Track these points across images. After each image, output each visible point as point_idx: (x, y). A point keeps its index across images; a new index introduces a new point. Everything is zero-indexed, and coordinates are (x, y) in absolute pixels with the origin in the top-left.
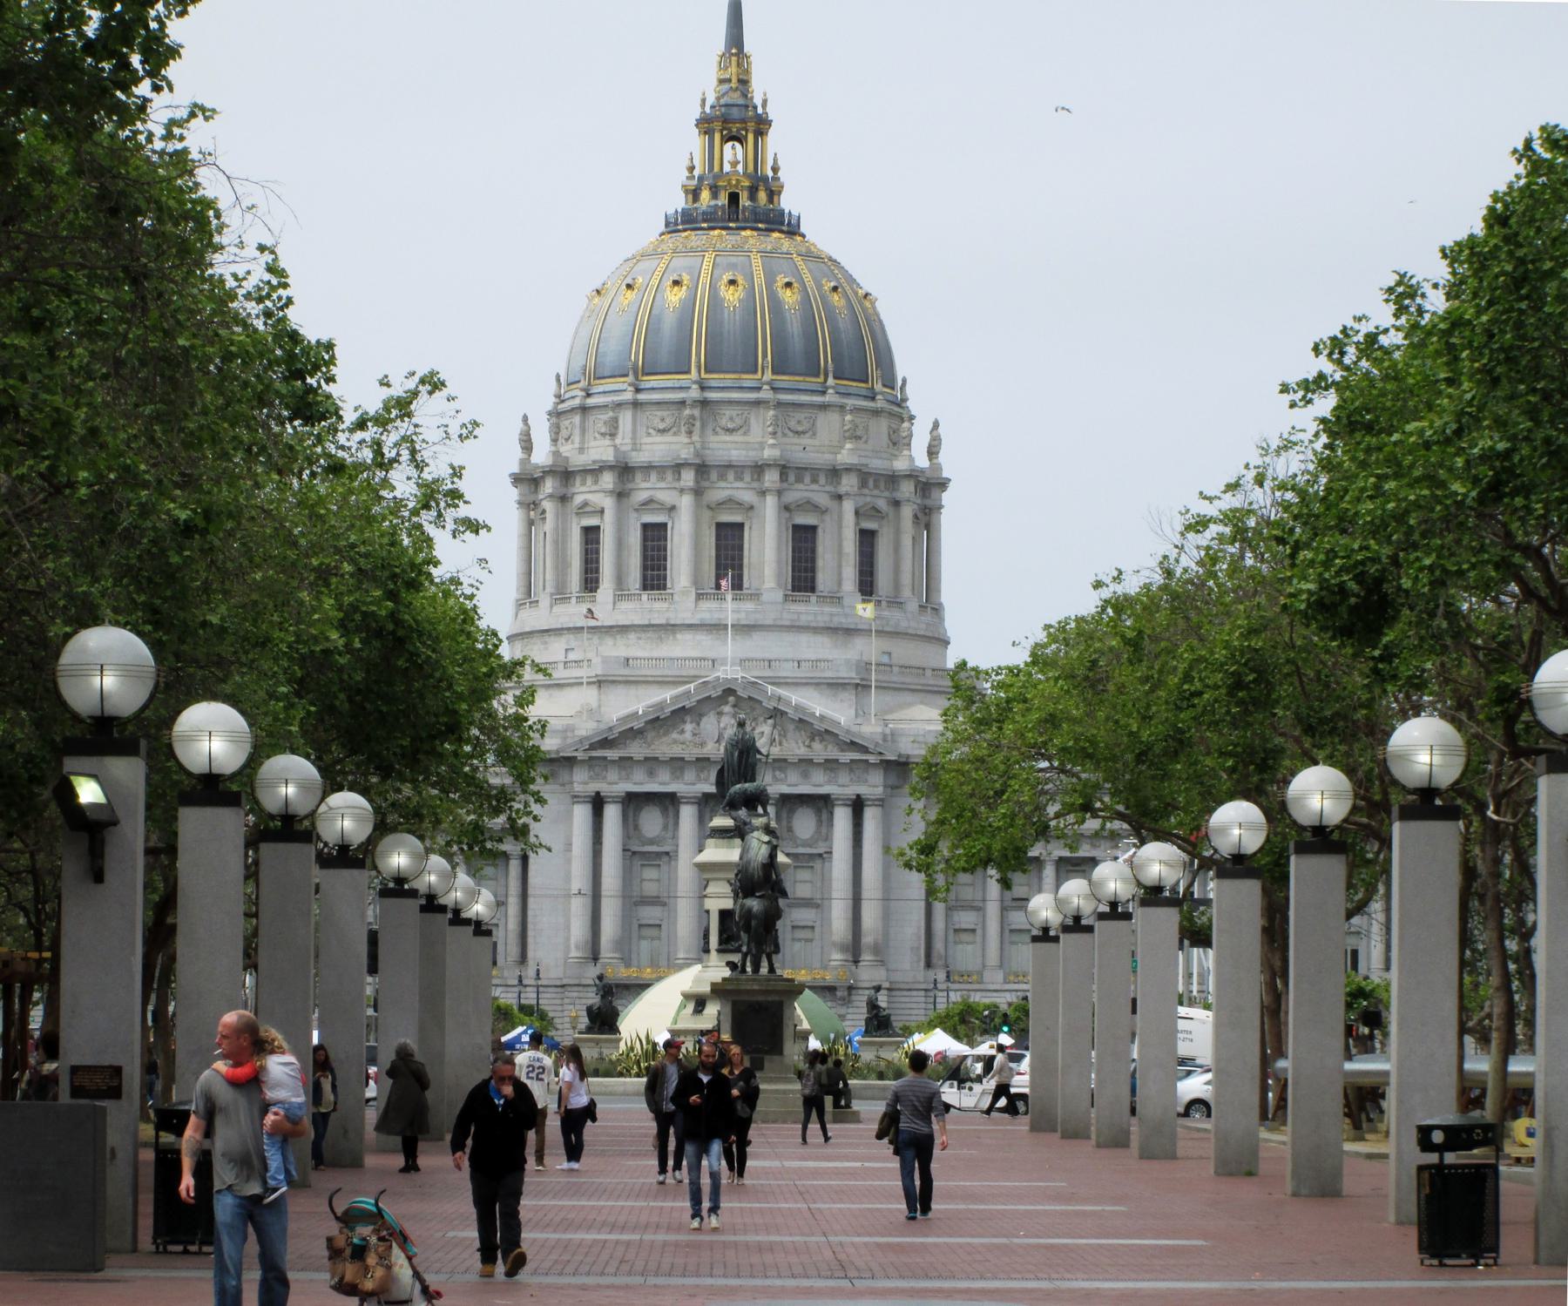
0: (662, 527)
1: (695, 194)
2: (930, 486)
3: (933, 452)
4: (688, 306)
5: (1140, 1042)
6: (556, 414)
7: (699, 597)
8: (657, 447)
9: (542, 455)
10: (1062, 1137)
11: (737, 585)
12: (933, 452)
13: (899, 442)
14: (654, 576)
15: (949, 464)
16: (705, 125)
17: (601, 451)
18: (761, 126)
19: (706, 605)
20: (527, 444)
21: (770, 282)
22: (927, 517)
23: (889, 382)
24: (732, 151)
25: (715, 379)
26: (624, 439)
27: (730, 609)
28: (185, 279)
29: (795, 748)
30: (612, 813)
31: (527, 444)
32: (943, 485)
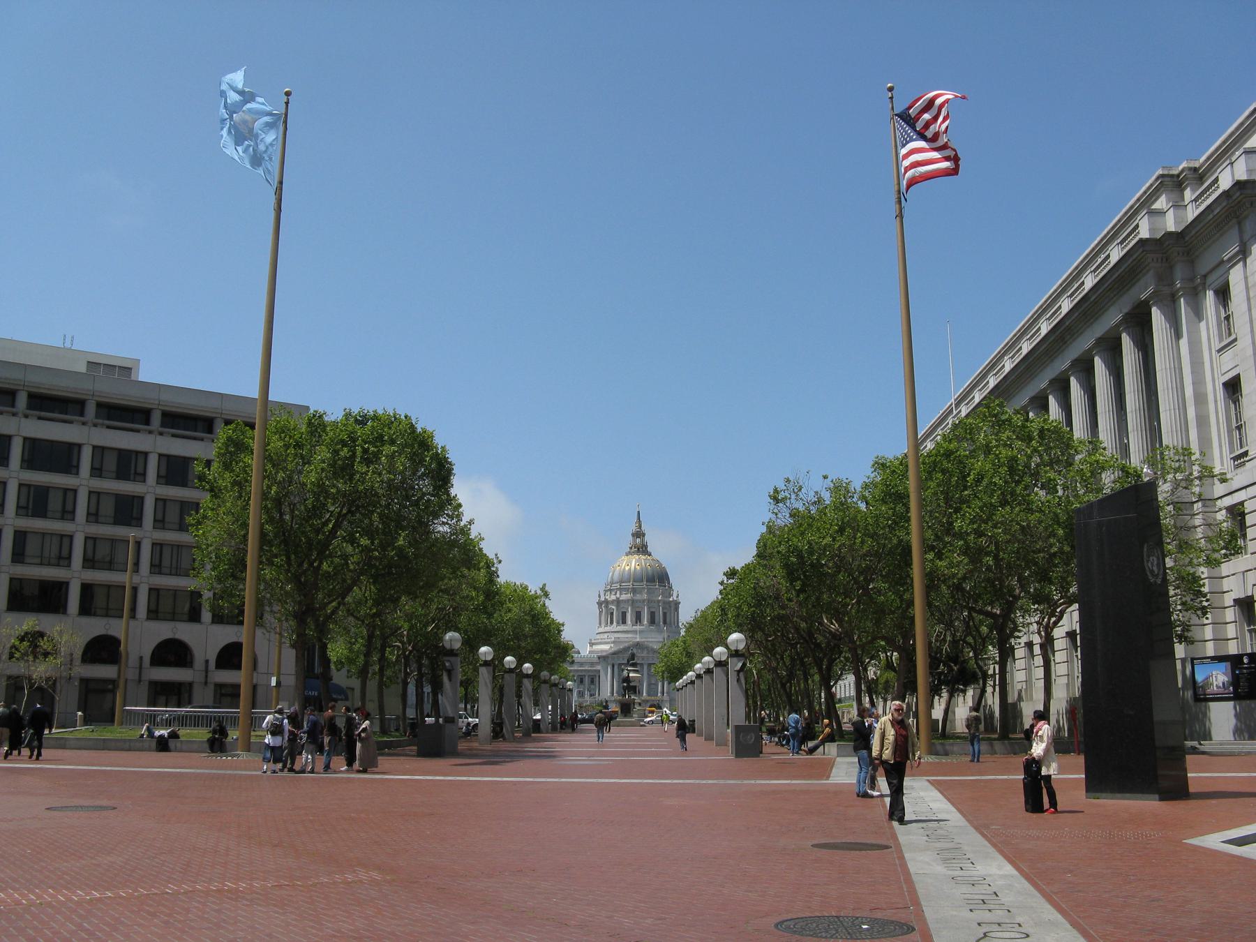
0: (640, 612)
1: (631, 548)
2: (677, 604)
3: (677, 597)
4: (630, 569)
5: (886, 807)
6: (606, 591)
7: (633, 625)
8: (624, 597)
9: (603, 599)
10: (705, 740)
11: (640, 622)
12: (677, 597)
13: (670, 595)
14: (624, 622)
15: (680, 599)
16: (633, 535)
17: (613, 597)
18: (644, 535)
19: (634, 627)
20: (600, 596)
21: (635, 564)
22: (677, 609)
23: (669, 583)
24: (638, 540)
25: (635, 584)
26: (618, 595)
27: (638, 628)
28: (1049, 431)
29: (645, 654)
30: (616, 667)
31: (600, 596)
32: (679, 603)
